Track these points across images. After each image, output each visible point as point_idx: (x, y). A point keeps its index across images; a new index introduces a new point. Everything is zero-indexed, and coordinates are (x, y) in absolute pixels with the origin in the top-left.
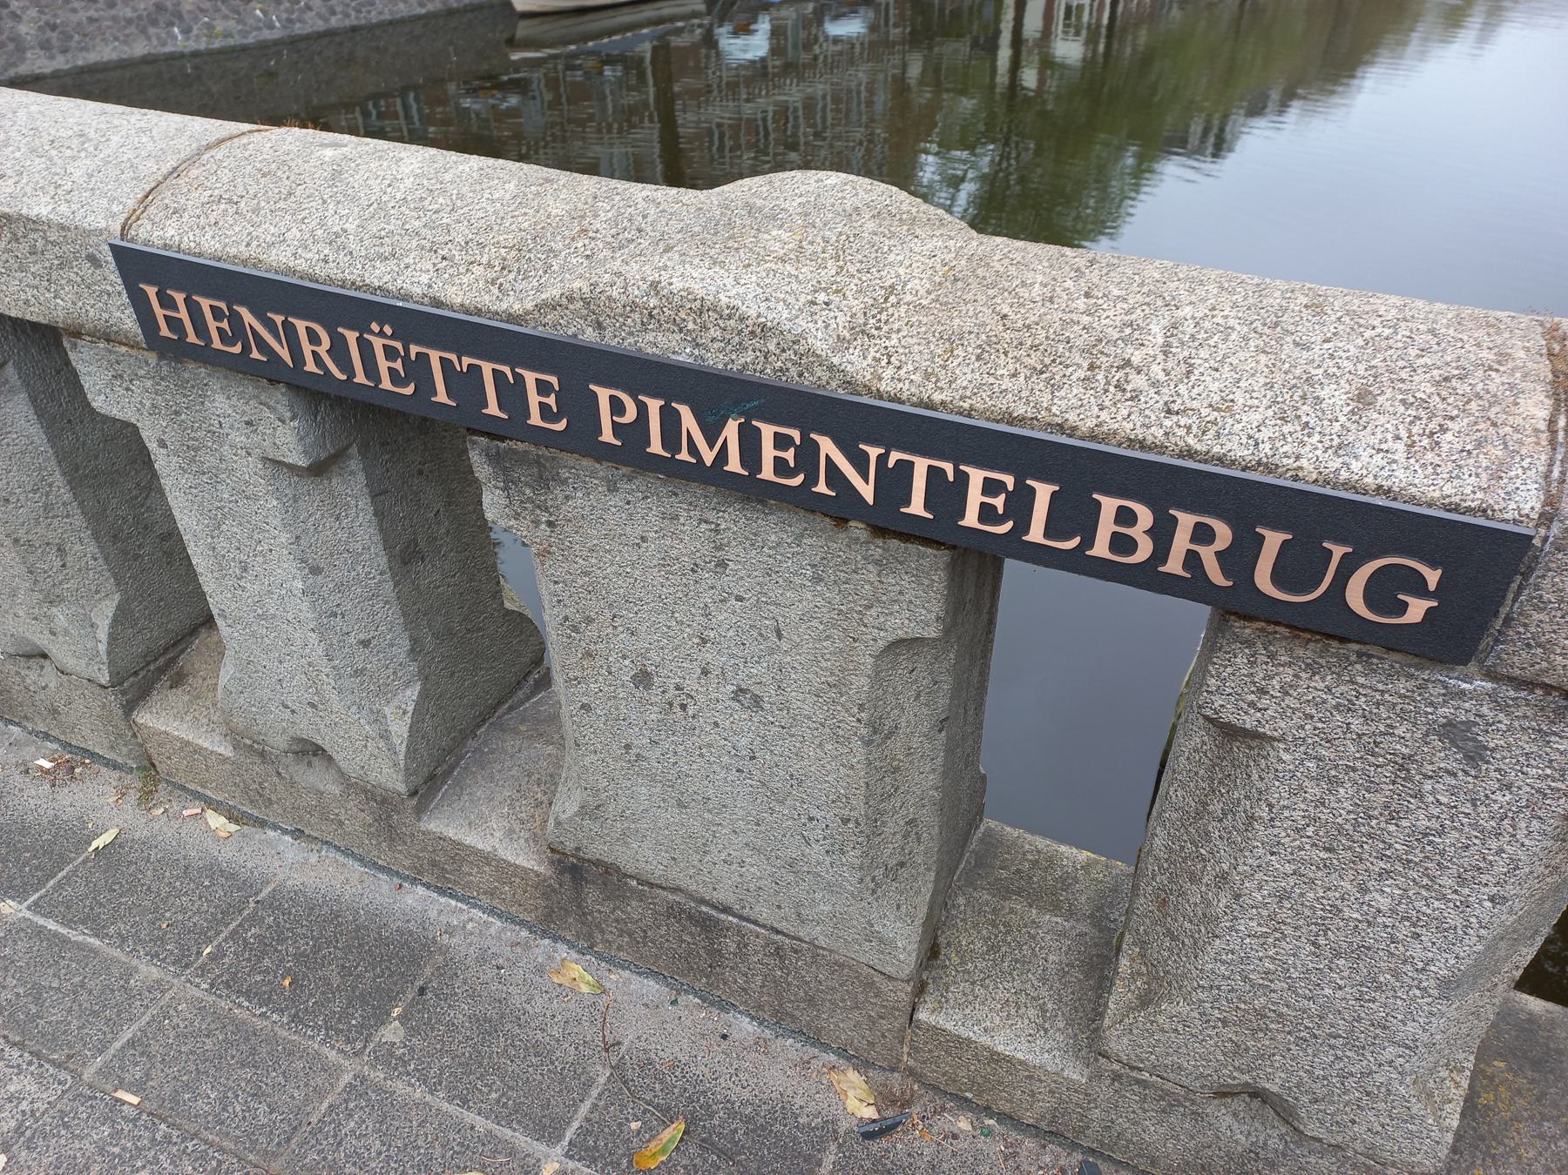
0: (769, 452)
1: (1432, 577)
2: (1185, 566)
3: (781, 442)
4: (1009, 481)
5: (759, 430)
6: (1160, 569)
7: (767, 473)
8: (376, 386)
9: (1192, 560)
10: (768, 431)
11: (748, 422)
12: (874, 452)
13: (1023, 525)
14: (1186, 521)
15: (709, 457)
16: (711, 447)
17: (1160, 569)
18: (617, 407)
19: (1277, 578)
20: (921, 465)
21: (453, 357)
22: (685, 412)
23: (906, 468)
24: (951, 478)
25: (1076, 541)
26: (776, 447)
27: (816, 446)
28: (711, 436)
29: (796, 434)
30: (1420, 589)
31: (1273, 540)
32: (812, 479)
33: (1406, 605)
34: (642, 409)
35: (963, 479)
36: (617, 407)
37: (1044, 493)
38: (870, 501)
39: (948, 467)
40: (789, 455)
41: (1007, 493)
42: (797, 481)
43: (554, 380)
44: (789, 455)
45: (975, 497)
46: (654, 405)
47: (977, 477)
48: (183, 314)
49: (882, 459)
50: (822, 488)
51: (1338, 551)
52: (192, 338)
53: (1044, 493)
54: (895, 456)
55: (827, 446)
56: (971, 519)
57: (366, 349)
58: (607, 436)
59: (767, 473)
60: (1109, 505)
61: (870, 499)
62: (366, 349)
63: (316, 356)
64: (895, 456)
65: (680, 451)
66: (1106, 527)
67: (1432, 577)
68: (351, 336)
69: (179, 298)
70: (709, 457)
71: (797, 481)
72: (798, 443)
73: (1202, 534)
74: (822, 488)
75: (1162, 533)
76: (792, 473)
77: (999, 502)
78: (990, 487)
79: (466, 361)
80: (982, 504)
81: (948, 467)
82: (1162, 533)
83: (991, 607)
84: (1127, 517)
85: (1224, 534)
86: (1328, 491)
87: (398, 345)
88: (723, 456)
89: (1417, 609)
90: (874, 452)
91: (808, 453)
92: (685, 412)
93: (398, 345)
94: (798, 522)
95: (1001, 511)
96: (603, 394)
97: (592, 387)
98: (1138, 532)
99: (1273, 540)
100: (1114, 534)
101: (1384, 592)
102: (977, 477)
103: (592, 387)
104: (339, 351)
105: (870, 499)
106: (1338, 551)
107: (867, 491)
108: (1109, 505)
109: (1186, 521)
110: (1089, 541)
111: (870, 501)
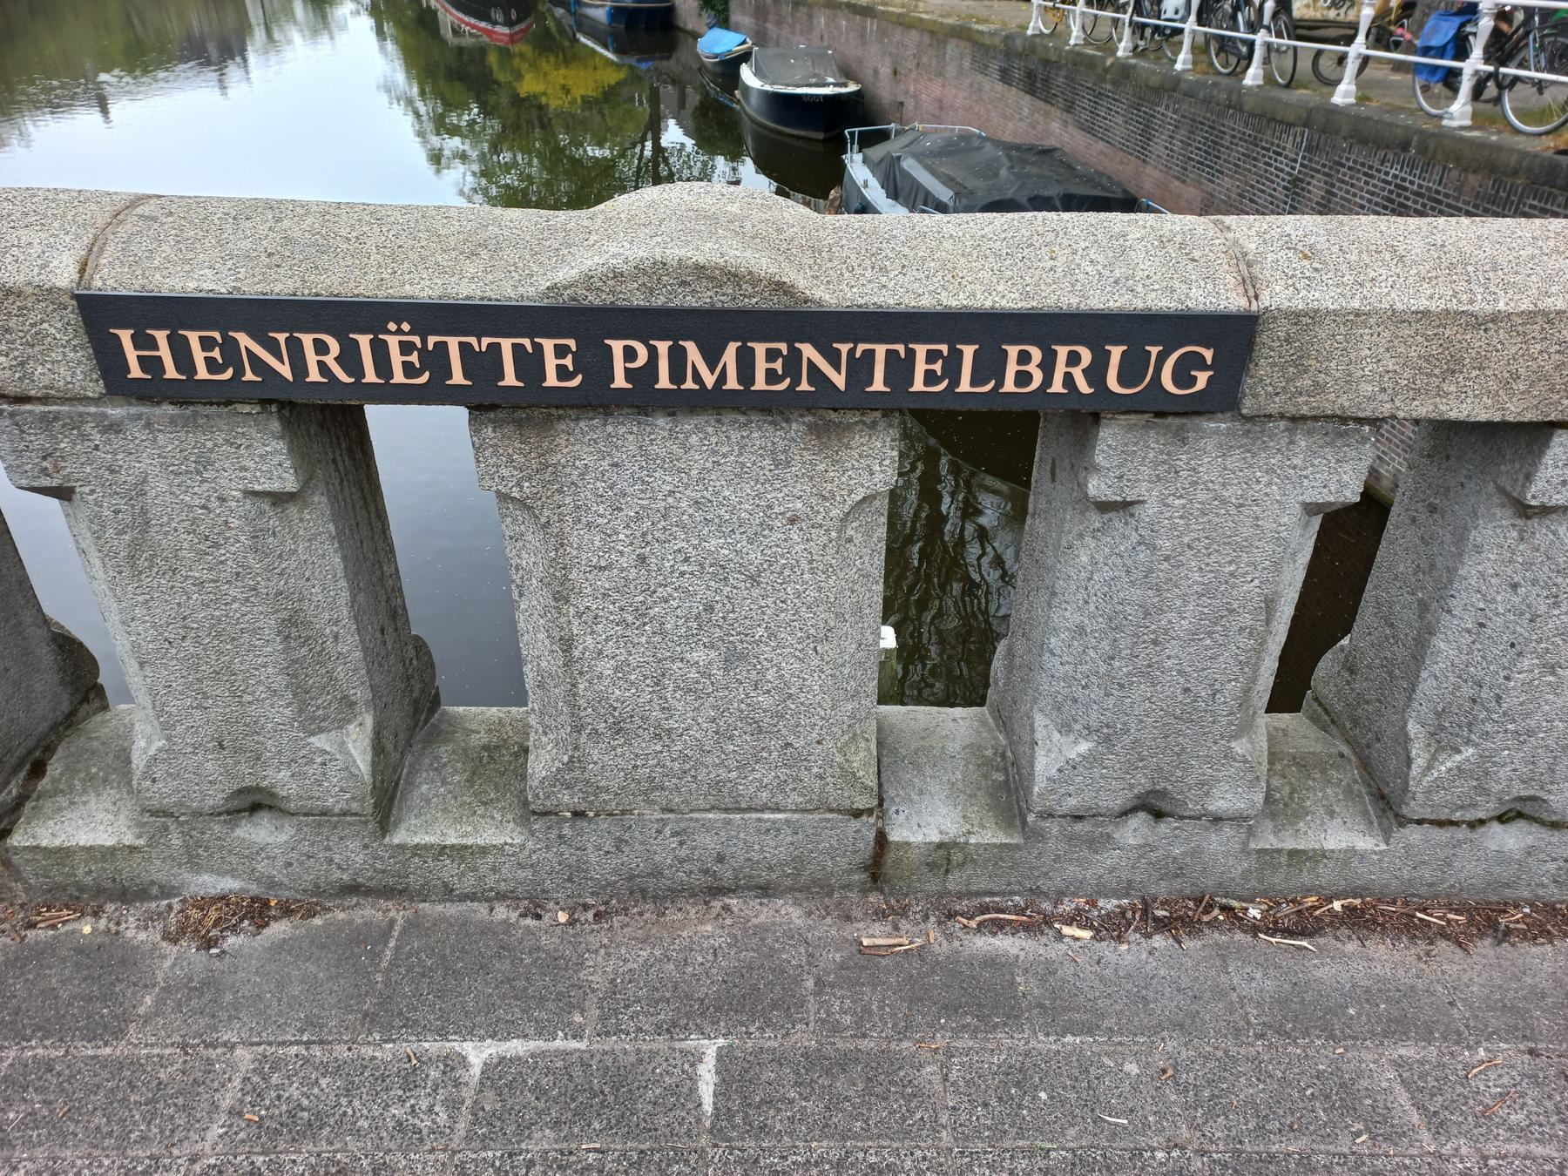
0: (199, 356)
1: (1208, 355)
2: (1064, 386)
3: (207, 344)
4: (783, 347)
5: (356, 341)
6: (868, 389)
7: (399, 377)
8: (387, 382)
9: (1069, 380)
10: (193, 337)
11: (744, 345)
12: (844, 348)
13: (956, 381)
14: (1062, 352)
15: (709, 380)
16: (712, 372)
17: (868, 389)
18: (630, 354)
19: (1121, 381)
20: (506, 344)
21: (473, 340)
22: (691, 348)
23: (442, 348)
24: (530, 350)
25: (993, 383)
26: (402, 354)
27: (800, 352)
28: (712, 359)
29: (217, 335)
30: (1202, 366)
31: (1116, 352)
32: (239, 372)
33: (1196, 377)
34: (653, 353)
35: (538, 348)
36: (630, 354)
37: (968, 351)
38: (290, 378)
39: (526, 342)
40: (216, 354)
41: (783, 356)
42: (229, 374)
43: (572, 343)
44: (216, 354)
45: (551, 363)
46: (663, 347)
47: (548, 345)
48: (164, 352)
49: (851, 352)
50: (249, 376)
51: (1154, 350)
52: (171, 372)
53: (968, 351)
54: (861, 347)
55: (244, 340)
56: (551, 380)
57: (380, 350)
58: (620, 381)
59: (399, 377)
60: (1013, 351)
61: (842, 386)
62: (380, 350)
63: (323, 367)
64: (861, 347)
65: (684, 381)
66: (1012, 368)
67: (1208, 355)
68: (364, 341)
69: (161, 336)
70: (709, 380)
71: (229, 374)
72: (220, 341)
73: (1074, 359)
74: (249, 376)
75: (1048, 366)
76: (222, 369)
77: (937, 367)
78: (772, 355)
79: (486, 341)
80: (404, 363)
81: (526, 342)
82: (1048, 366)
83: (377, 510)
84: (1024, 358)
85: (1086, 356)
86: (201, 295)
87: (416, 340)
88: (722, 378)
89: (1202, 379)
90: (844, 348)
91: (230, 348)
92: (691, 348)
93: (416, 340)
94: (761, 436)
95: (571, 369)
96: (617, 346)
97: (835, 345)
98: (1032, 368)
99: (1116, 352)
100: (1018, 373)
101: (1183, 376)
102: (548, 345)
103: (835, 345)
104: (350, 358)
105: (842, 386)
106: (1154, 350)
107: (839, 380)
108: (1013, 351)
109: (1062, 352)
110: (1000, 383)
111: (290, 378)
